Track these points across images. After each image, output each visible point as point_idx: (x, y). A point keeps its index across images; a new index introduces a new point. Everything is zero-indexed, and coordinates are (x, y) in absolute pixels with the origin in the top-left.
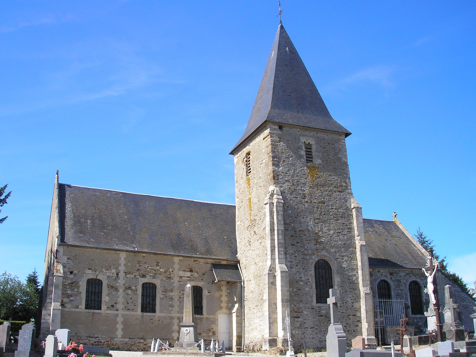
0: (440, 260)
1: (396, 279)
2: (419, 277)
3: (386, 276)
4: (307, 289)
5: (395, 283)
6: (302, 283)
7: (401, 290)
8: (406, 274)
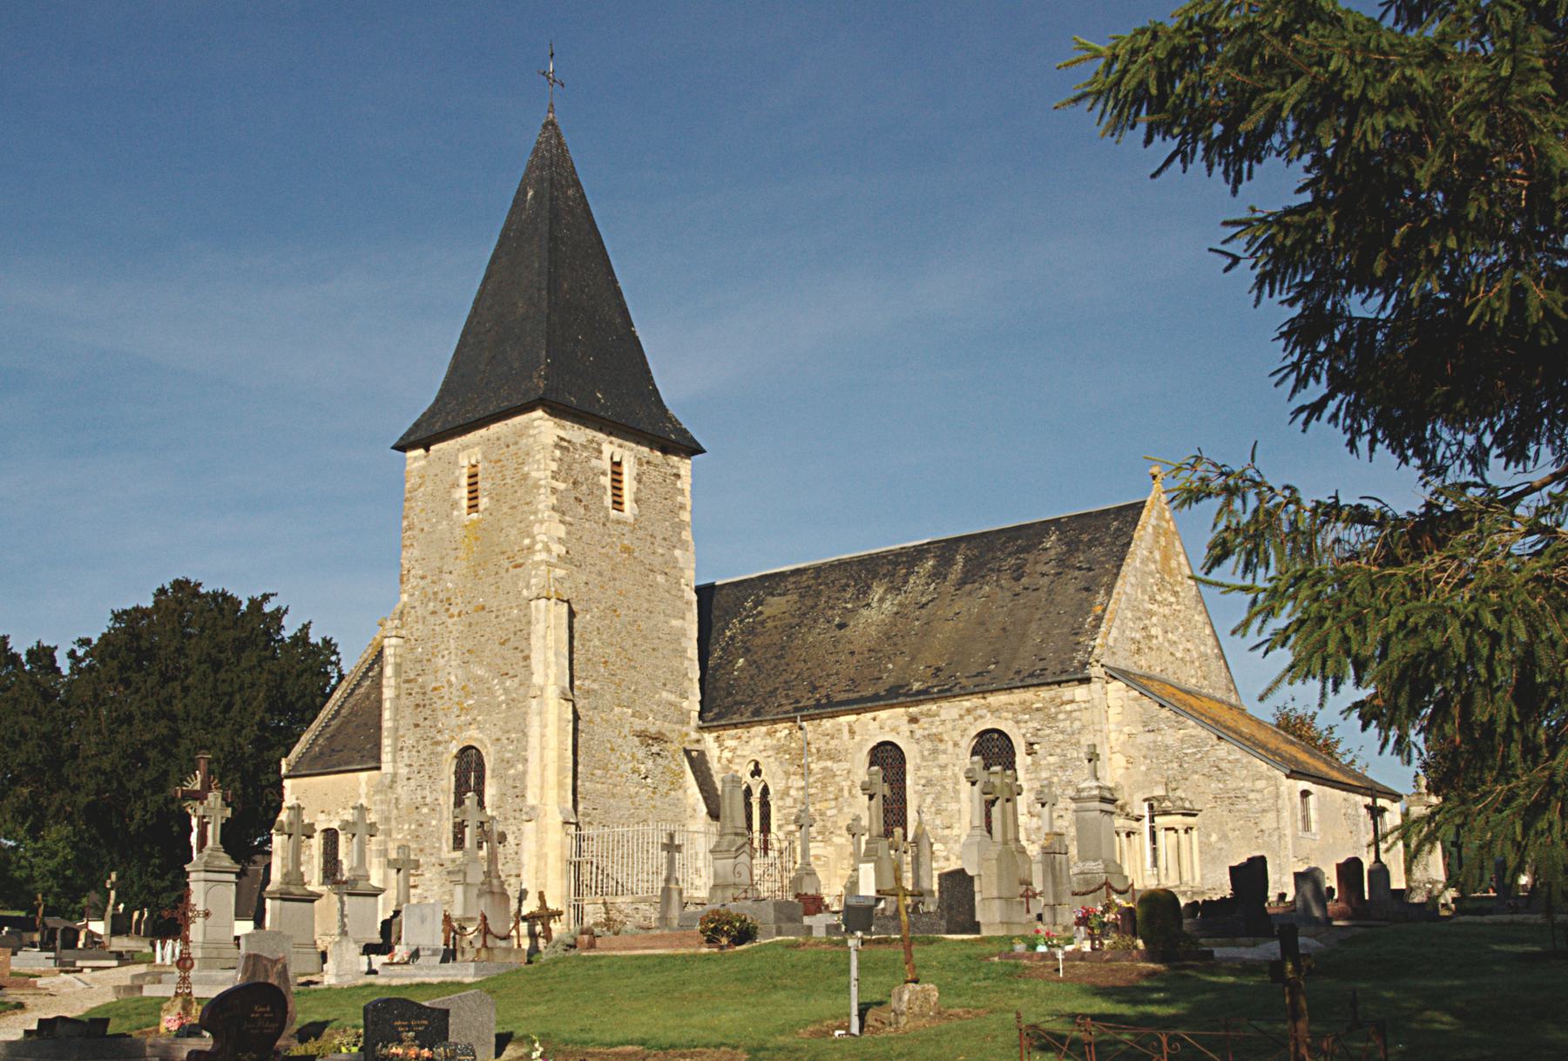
0: (75, 647)
1: (926, 732)
2: (1010, 715)
3: (895, 730)
4: (434, 823)
5: (923, 747)
6: (425, 810)
7: (943, 767)
8: (963, 712)
